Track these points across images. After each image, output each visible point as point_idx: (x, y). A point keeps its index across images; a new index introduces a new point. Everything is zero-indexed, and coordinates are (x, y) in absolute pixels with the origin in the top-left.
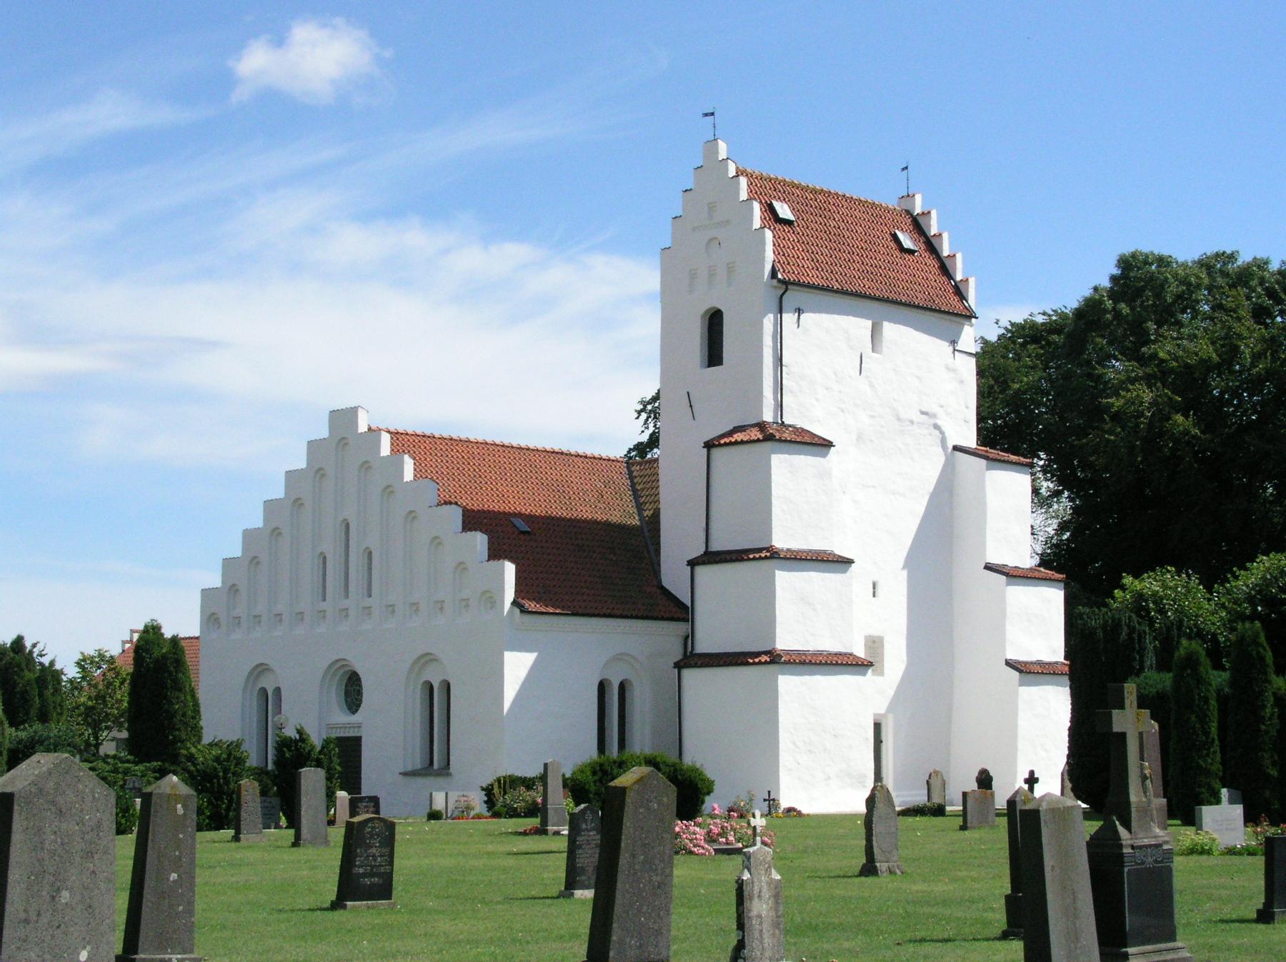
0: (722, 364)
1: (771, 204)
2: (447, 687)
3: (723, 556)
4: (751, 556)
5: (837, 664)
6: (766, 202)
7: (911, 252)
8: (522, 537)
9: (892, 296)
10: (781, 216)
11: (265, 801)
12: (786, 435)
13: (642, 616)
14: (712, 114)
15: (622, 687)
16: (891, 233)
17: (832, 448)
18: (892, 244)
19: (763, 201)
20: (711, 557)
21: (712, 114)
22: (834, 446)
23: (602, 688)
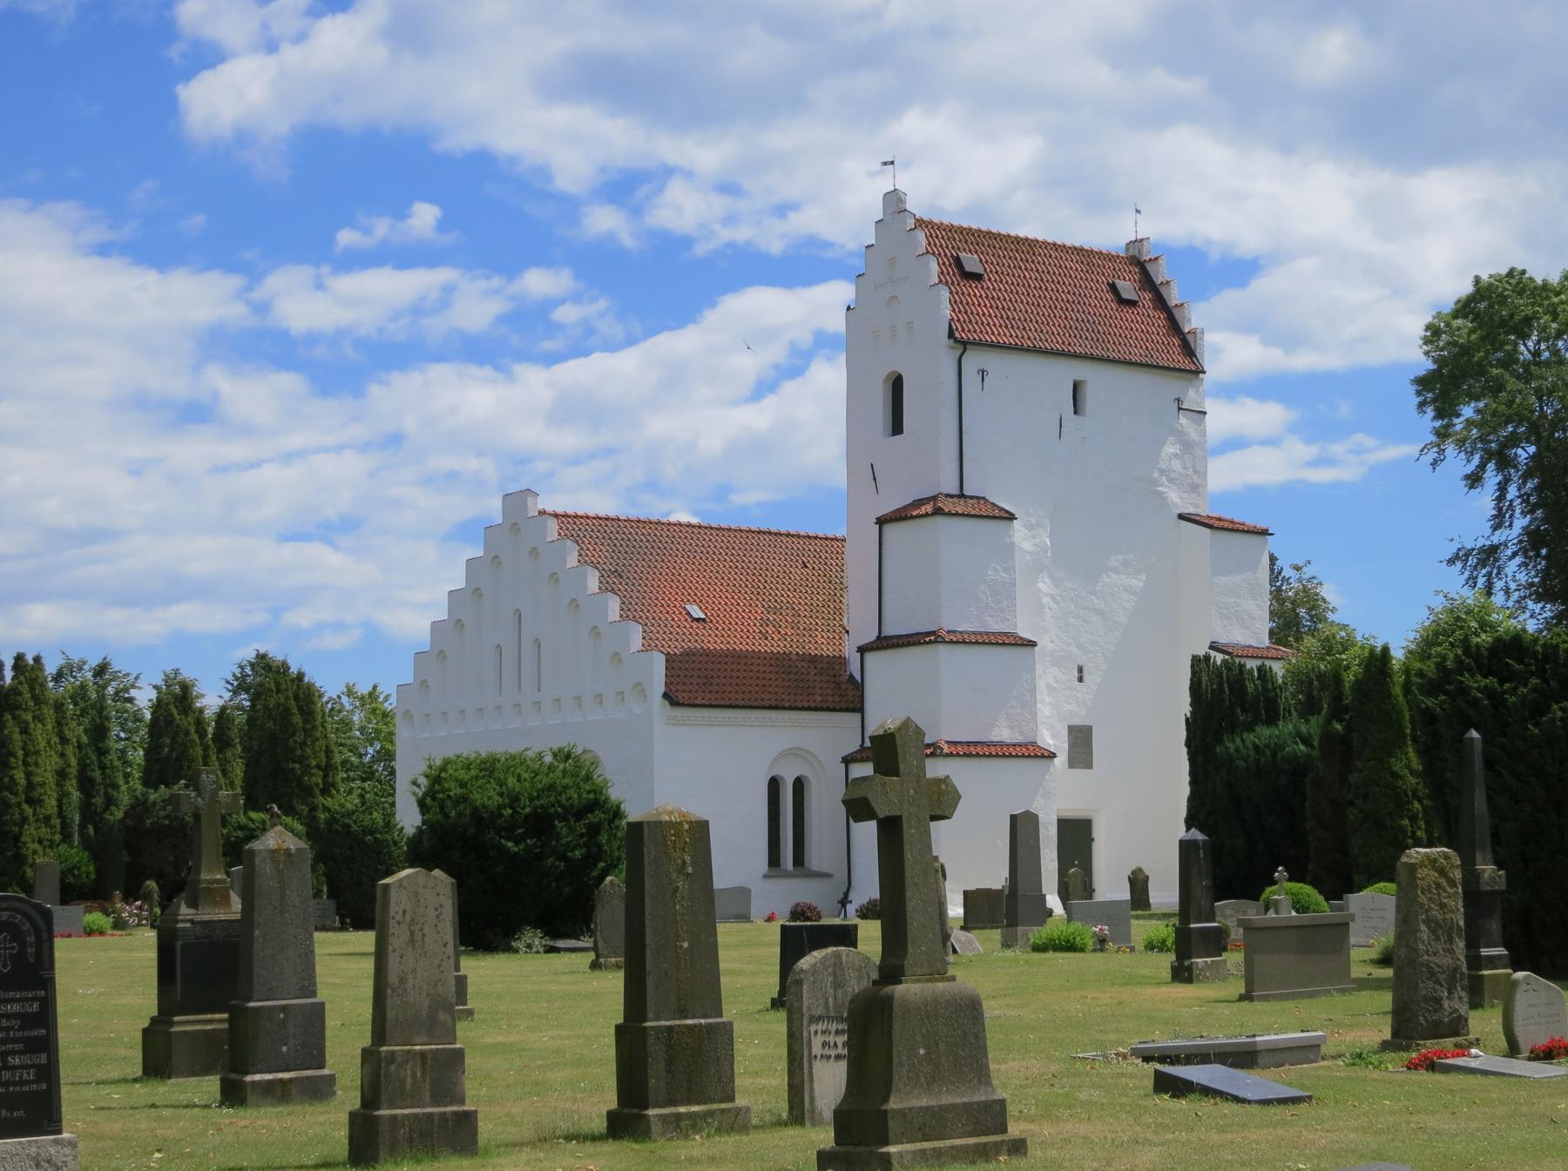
0: (902, 433)
1: (958, 257)
2: (799, 785)
3: (916, 639)
4: (927, 639)
5: (1010, 755)
6: (952, 255)
7: (1132, 303)
8: (695, 625)
9: (1095, 352)
10: (967, 269)
11: (318, 903)
12: (957, 509)
13: (803, 707)
14: (892, 163)
15: (799, 785)
16: (1108, 284)
17: (1015, 521)
18: (1110, 296)
19: (949, 255)
20: (885, 643)
21: (892, 163)
22: (1016, 519)
23: (774, 785)
